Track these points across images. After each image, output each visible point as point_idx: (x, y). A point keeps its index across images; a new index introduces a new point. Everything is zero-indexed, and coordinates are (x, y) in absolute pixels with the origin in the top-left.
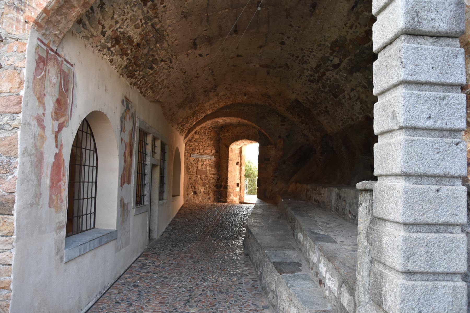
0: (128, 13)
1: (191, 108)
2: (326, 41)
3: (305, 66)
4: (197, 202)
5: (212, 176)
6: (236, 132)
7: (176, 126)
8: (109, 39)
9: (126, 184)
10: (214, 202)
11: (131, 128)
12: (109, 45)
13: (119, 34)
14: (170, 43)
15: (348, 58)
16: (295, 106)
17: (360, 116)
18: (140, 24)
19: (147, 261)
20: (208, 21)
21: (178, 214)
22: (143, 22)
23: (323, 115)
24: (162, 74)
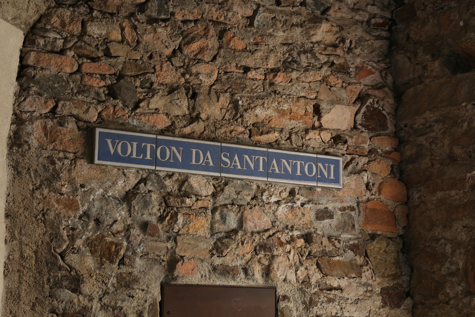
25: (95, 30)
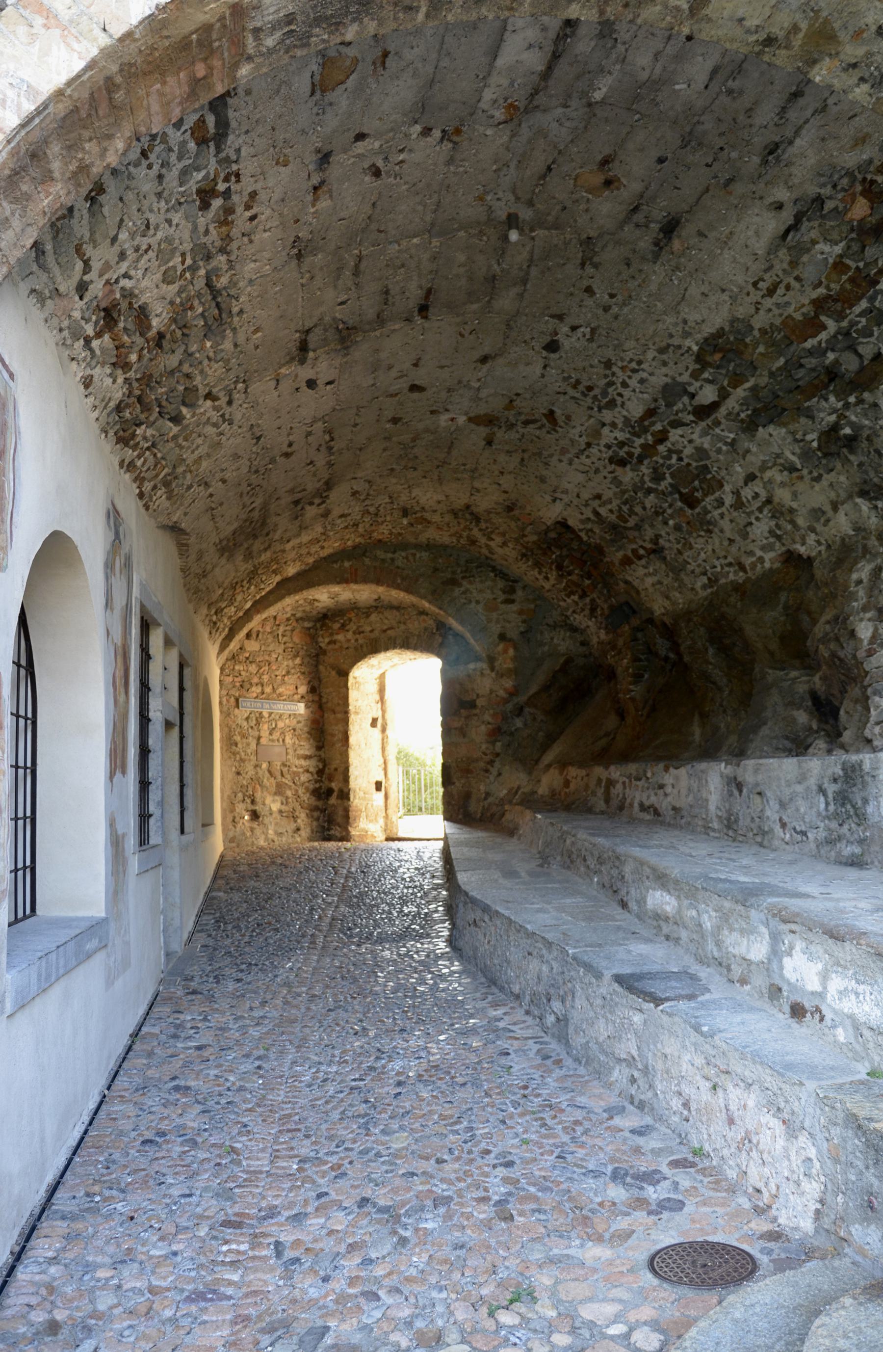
0: (157, 228)
1: (249, 555)
2: (686, 335)
3: (607, 416)
4: (262, 842)
5: (303, 763)
6: (369, 629)
7: (204, 611)
8: (91, 311)
9: (118, 774)
10: (311, 839)
11: (124, 603)
12: (90, 330)
13: (118, 296)
14: (241, 338)
15: (747, 385)
16: (559, 545)
17: (768, 556)
18: (180, 268)
19: (182, 1017)
20: (356, 272)
21: (215, 878)
22: (189, 262)
23: (643, 562)
24: (200, 441)
25: (237, 667)
